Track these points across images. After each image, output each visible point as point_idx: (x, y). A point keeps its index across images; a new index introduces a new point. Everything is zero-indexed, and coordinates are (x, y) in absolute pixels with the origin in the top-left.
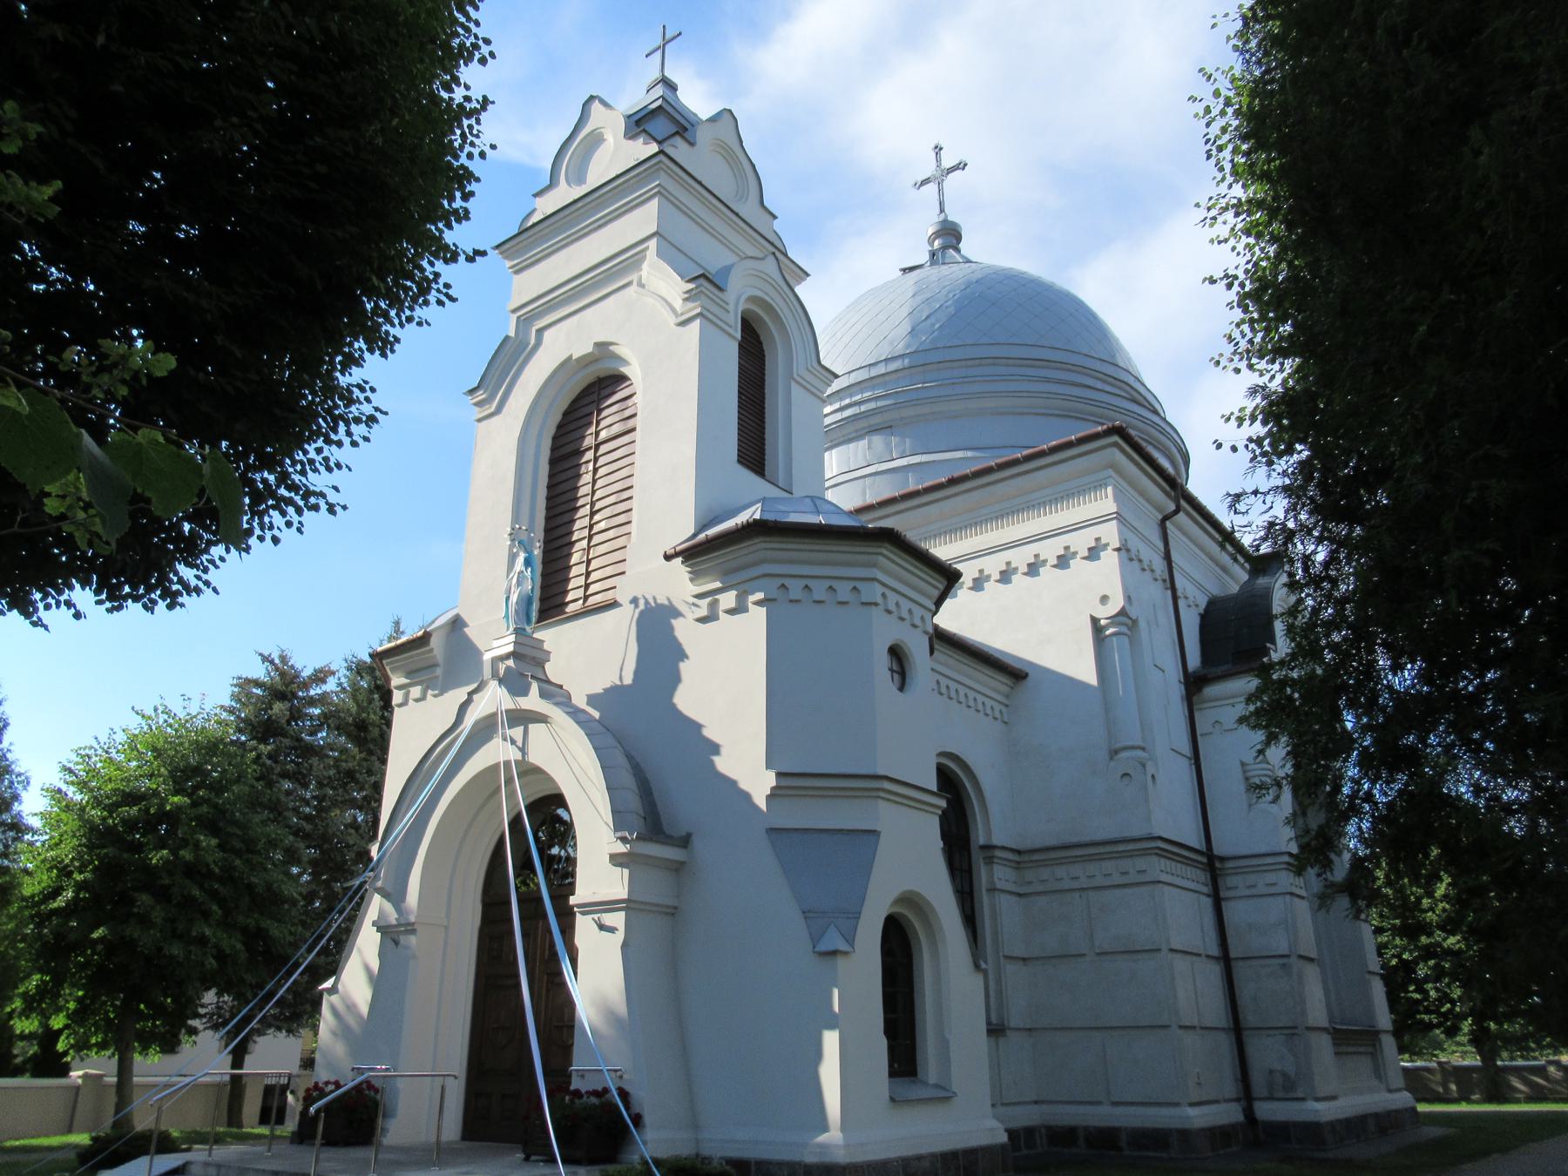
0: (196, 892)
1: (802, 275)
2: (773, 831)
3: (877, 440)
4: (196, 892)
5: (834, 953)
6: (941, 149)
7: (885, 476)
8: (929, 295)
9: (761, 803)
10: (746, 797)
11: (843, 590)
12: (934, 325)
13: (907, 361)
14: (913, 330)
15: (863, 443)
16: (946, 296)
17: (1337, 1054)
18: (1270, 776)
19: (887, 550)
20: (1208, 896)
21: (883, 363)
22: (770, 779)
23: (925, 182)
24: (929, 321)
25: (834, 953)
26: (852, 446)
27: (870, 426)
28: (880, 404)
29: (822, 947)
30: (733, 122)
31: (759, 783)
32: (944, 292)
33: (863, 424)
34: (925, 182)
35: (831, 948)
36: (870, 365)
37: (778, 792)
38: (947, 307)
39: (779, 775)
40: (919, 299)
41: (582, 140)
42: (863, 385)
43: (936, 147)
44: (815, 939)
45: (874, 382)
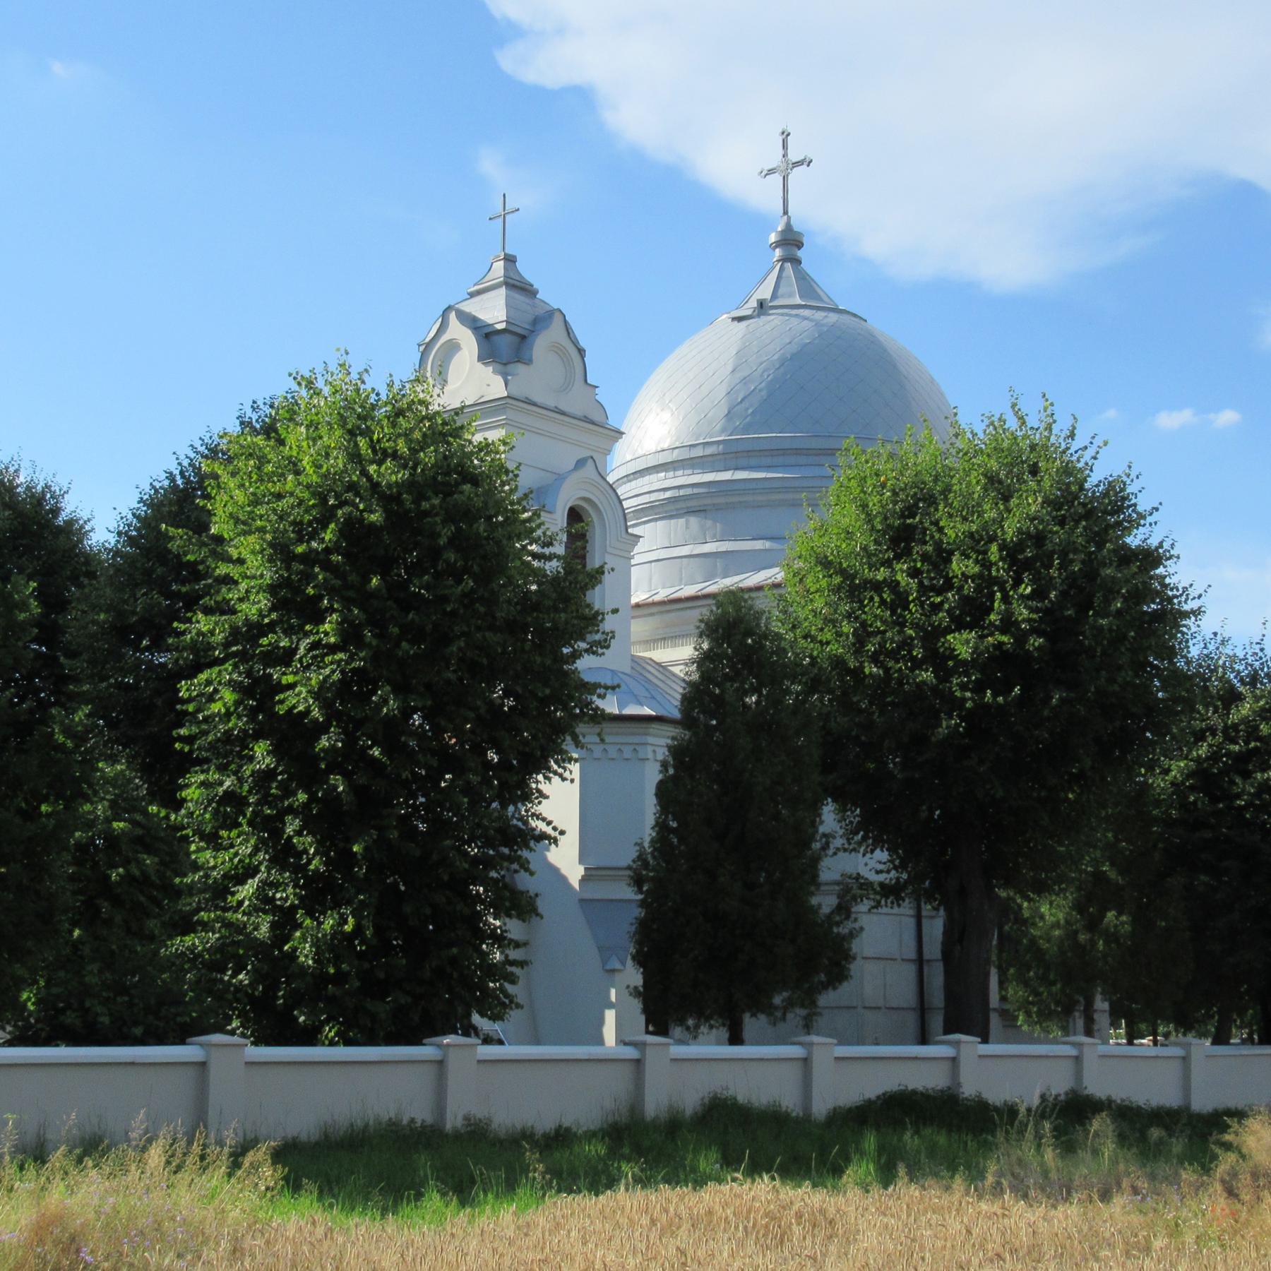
0: (142, 899)
1: (617, 435)
2: (582, 901)
3: (694, 520)
4: (142, 899)
5: (613, 971)
6: (789, 135)
7: (696, 559)
8: (746, 374)
9: (576, 885)
10: (563, 879)
11: (627, 752)
12: (748, 409)
13: (721, 447)
14: (729, 412)
15: (682, 521)
16: (762, 375)
17: (1004, 1026)
18: (487, 1040)
19: (655, 736)
20: (912, 916)
21: (701, 446)
22: (580, 871)
23: (771, 172)
24: (743, 405)
25: (613, 971)
26: (673, 521)
27: (688, 508)
28: (696, 491)
29: (608, 967)
30: (561, 316)
31: (574, 872)
32: (760, 371)
33: (681, 505)
34: (771, 172)
35: (612, 968)
36: (691, 446)
37: (594, 873)
38: (760, 391)
39: (585, 869)
40: (739, 375)
41: (443, 345)
42: (676, 465)
43: (783, 133)
44: (604, 962)
45: (695, 461)
